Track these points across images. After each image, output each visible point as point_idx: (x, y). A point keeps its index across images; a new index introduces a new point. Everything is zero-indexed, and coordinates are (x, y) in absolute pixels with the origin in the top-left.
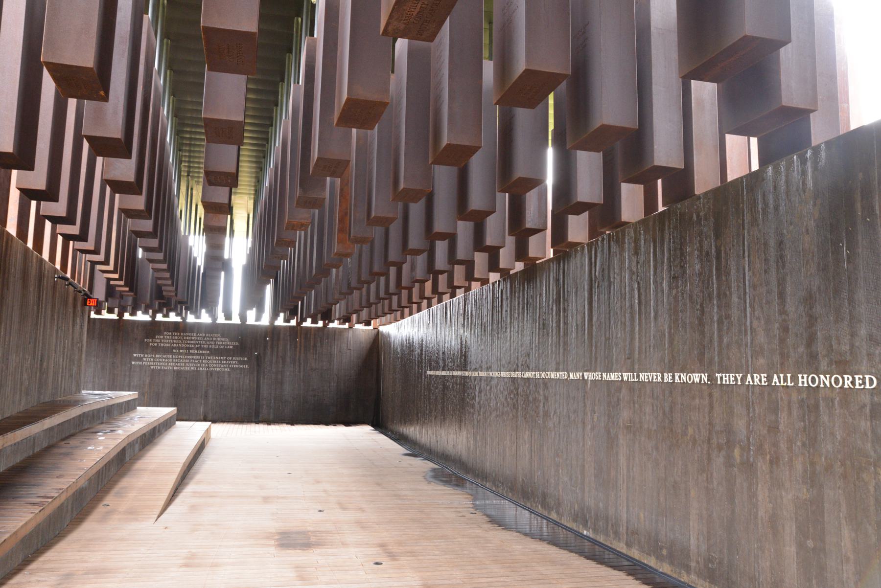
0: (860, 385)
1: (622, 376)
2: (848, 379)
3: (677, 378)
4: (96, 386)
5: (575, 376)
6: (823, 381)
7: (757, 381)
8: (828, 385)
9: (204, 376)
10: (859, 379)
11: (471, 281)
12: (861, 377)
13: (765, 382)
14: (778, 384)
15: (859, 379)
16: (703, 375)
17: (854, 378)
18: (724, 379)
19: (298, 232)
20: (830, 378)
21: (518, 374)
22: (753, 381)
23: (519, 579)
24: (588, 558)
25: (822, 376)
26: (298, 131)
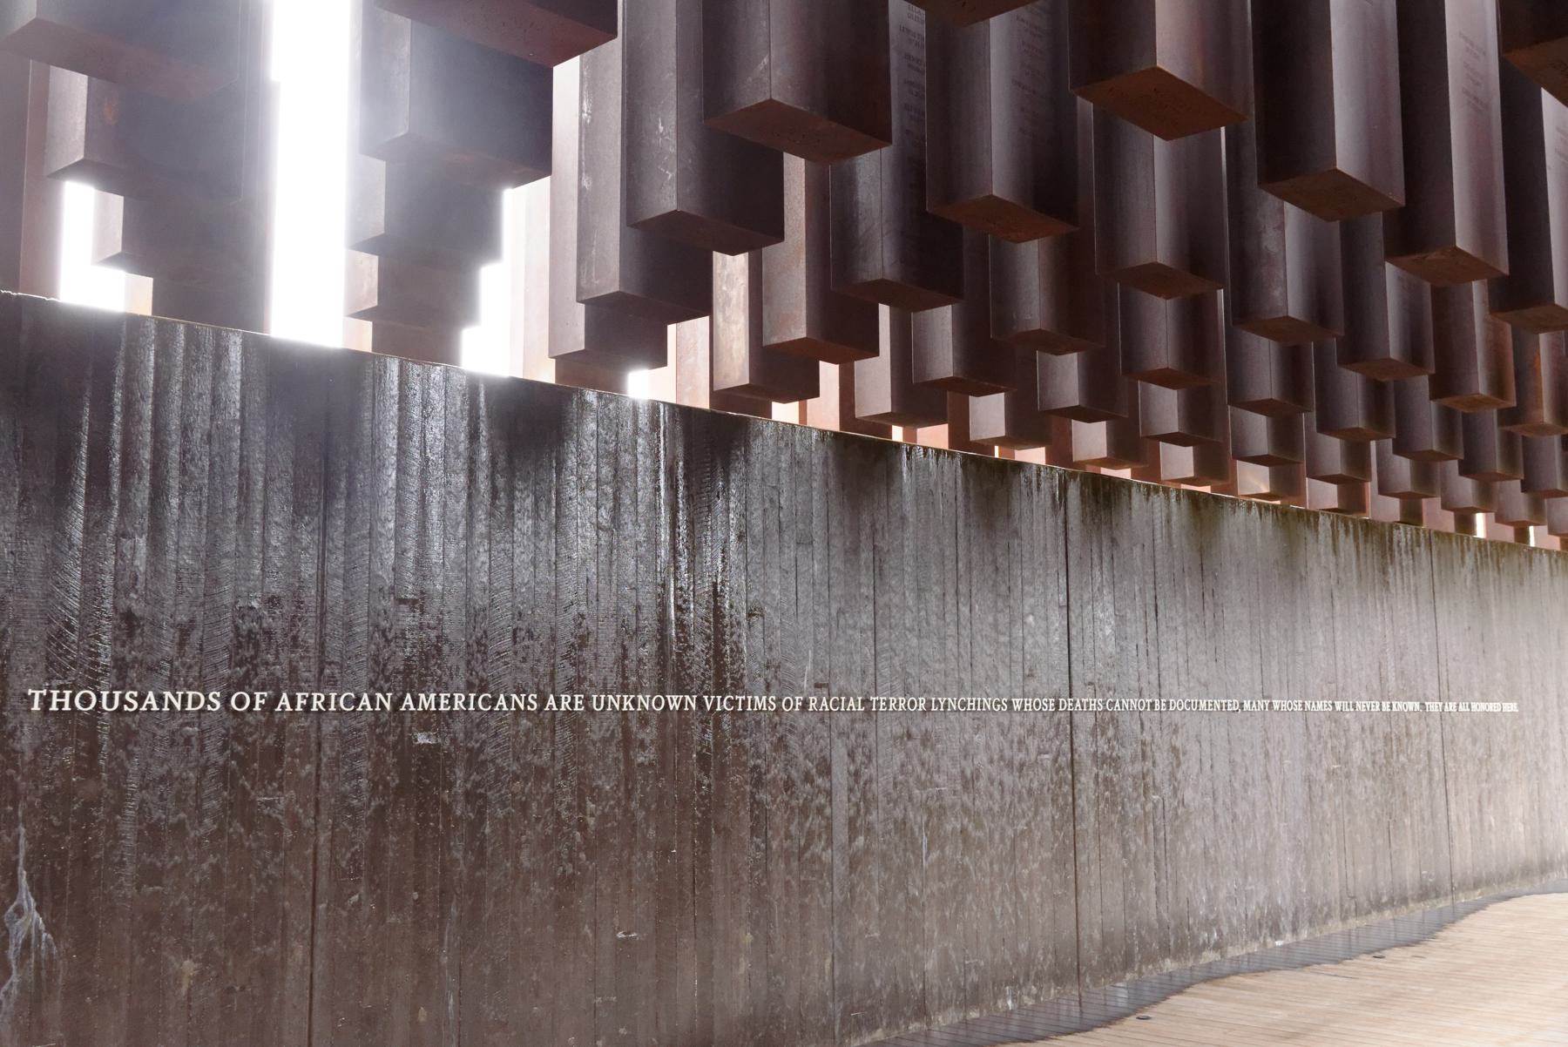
0: (445, 706)
1: (1333, 704)
2: (319, 698)
3: (1394, 706)
4: (669, 682)
5: (1254, 705)
6: (169, 700)
7: (565, 705)
8: (647, 707)
9: (668, 689)
10: (304, 697)
11: (760, 247)
12: (449, 695)
13: (580, 706)
14: (854, 709)
15: (304, 697)
16: (687, 697)
17: (573, 698)
18: (1026, 705)
19: (1373, 444)
20: (651, 699)
21: (106, 699)
22: (558, 705)
23: (1154, 629)
24: (1165, 999)
25: (610, 697)
26: (1216, 316)
